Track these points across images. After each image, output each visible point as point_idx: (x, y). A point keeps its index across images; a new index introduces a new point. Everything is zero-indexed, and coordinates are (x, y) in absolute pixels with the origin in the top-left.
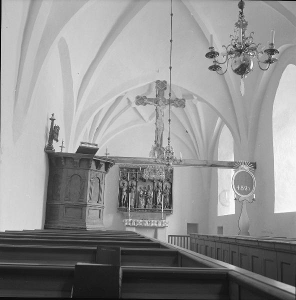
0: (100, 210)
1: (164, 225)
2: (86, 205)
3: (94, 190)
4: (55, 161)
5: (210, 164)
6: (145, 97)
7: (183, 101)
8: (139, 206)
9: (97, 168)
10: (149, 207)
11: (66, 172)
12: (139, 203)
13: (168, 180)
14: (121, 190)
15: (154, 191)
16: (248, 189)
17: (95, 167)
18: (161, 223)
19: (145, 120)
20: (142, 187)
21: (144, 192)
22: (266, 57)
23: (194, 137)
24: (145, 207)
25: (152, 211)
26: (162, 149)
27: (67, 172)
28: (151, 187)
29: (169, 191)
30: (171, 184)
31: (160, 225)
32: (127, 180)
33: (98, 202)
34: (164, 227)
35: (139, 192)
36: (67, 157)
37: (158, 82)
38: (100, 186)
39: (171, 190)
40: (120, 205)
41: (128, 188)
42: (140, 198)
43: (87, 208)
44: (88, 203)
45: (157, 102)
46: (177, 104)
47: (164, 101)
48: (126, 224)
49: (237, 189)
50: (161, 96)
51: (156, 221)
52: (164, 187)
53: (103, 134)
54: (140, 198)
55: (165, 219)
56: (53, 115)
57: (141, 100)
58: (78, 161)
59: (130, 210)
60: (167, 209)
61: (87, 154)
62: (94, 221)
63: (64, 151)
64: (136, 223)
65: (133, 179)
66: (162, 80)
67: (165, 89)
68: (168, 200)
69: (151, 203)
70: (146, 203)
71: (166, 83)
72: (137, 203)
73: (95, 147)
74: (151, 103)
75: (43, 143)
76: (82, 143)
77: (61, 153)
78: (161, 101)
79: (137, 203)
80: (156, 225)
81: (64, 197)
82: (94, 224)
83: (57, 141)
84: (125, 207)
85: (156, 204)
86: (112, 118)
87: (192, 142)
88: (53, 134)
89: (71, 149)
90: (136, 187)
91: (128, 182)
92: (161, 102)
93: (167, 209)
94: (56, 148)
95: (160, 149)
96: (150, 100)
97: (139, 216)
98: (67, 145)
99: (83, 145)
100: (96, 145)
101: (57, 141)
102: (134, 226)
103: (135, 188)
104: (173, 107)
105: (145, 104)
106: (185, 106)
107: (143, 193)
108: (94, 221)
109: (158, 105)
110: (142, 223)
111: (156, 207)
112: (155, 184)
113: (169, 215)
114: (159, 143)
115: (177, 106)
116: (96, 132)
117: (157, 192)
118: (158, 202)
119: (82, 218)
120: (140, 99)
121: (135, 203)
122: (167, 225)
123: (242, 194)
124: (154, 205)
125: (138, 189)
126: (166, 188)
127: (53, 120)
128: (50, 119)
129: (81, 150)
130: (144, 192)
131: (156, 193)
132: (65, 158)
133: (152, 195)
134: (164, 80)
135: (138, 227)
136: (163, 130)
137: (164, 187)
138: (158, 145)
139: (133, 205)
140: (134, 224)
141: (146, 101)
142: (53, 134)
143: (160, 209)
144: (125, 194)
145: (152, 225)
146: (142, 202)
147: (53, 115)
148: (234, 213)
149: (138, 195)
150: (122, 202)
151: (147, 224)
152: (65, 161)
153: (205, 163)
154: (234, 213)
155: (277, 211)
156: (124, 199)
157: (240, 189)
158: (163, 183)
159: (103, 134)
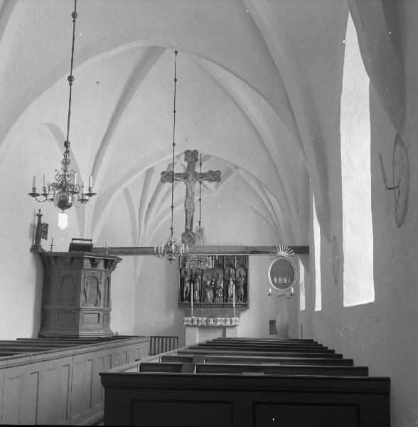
0: (99, 315)
1: (234, 324)
2: (79, 310)
3: (90, 292)
4: (46, 262)
8: (205, 300)
10: (220, 300)
12: (206, 295)
14: (182, 280)
15: (224, 280)
17: (90, 265)
18: (229, 321)
19: (208, 189)
21: (212, 281)
22: (42, 198)
23: (271, 205)
24: (213, 301)
26: (192, 235)
28: (221, 276)
29: (243, 280)
30: (247, 270)
32: (234, 268)
33: (95, 305)
35: (206, 282)
36: (58, 257)
37: (187, 152)
38: (98, 286)
39: (246, 278)
40: (182, 299)
41: (191, 277)
44: (82, 307)
46: (211, 177)
47: (195, 174)
48: (186, 323)
50: (192, 170)
51: (223, 319)
52: (238, 275)
55: (238, 316)
56: (40, 210)
57: (169, 176)
58: (69, 260)
60: (241, 303)
61: (80, 250)
62: (91, 326)
63: (54, 250)
64: (198, 321)
66: (191, 149)
67: (196, 160)
68: (242, 291)
69: (220, 295)
70: (215, 295)
71: (197, 153)
72: (203, 295)
74: (179, 179)
75: (29, 243)
76: (73, 239)
77: (51, 252)
80: (223, 324)
82: (90, 330)
83: (46, 239)
85: (227, 297)
87: (270, 213)
89: (62, 247)
90: (202, 276)
92: (191, 177)
93: (241, 303)
94: (45, 245)
95: (189, 236)
96: (179, 175)
97: (206, 313)
99: (74, 242)
100: (91, 240)
101: (46, 239)
102: (195, 326)
103: (200, 277)
104: (206, 182)
106: (220, 179)
107: (211, 284)
108: (91, 326)
110: (206, 321)
112: (226, 271)
114: (189, 227)
115: (210, 180)
116: (148, 210)
117: (229, 281)
118: (230, 295)
119: (75, 324)
121: (200, 294)
122: (237, 324)
123: (281, 288)
124: (225, 297)
125: (205, 279)
126: (240, 276)
127: (40, 216)
128: (37, 215)
129: (73, 247)
130: (212, 281)
131: (227, 283)
132: (55, 257)
133: (222, 285)
134: (195, 149)
137: (238, 275)
138: (187, 230)
139: (197, 298)
140: (196, 323)
144: (188, 285)
145: (219, 324)
146: (210, 295)
147: (40, 210)
148: (371, 299)
149: (204, 286)
151: (212, 322)
152: (56, 262)
153: (244, 250)
154: (371, 299)
155: (346, 304)
156: (187, 291)
158: (235, 269)
159: (157, 213)
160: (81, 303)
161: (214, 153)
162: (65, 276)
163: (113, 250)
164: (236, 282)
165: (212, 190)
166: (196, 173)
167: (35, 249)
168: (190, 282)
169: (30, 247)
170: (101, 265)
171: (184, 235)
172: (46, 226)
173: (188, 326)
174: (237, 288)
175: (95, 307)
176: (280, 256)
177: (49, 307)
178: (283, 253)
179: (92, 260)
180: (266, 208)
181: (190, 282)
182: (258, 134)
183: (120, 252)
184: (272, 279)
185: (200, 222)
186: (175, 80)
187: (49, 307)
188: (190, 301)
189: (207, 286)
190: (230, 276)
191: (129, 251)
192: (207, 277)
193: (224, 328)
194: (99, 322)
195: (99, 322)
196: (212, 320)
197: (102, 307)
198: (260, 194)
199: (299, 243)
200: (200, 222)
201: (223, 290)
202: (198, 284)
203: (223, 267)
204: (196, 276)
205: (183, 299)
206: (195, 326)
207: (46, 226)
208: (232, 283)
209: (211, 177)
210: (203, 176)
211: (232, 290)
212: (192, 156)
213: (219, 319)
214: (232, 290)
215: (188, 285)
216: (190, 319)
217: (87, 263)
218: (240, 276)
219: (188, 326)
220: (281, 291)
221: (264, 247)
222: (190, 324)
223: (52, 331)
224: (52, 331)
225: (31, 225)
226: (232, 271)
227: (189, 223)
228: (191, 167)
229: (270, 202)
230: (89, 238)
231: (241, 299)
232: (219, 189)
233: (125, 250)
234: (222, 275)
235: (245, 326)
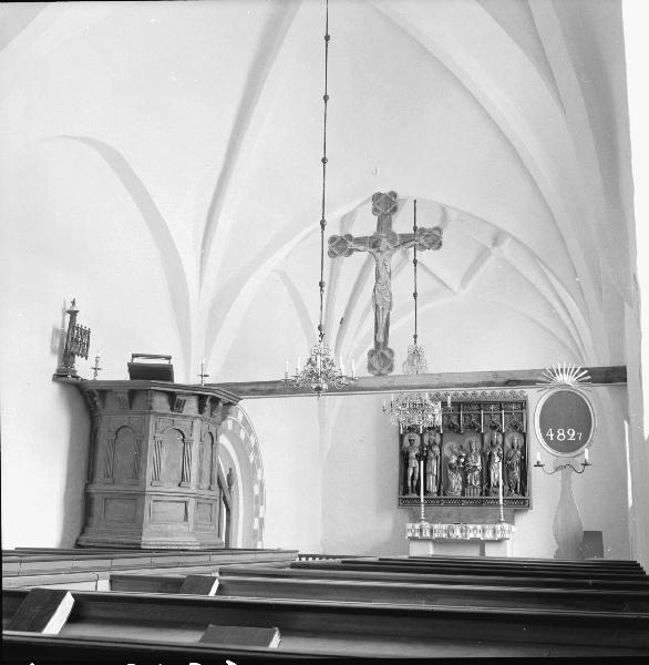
2: (142, 494)
4: (88, 400)
5: (503, 380)
6: (349, 237)
7: (437, 233)
9: (172, 409)
11: (111, 418)
12: (448, 484)
13: (516, 427)
14: (405, 458)
15: (483, 455)
16: (576, 436)
18: (491, 532)
19: (450, 289)
20: (455, 445)
24: (463, 493)
25: (480, 503)
26: (386, 353)
27: (120, 418)
28: (476, 445)
29: (519, 452)
30: (525, 435)
31: (489, 536)
32: (500, 431)
34: (500, 541)
39: (524, 449)
40: (406, 491)
41: (421, 450)
42: (449, 472)
43: (148, 501)
44: (148, 488)
45: (375, 245)
46: (422, 241)
47: (392, 237)
48: (410, 535)
49: (547, 439)
51: (479, 527)
52: (508, 444)
53: (357, 333)
54: (449, 472)
55: (511, 521)
56: (73, 303)
58: (126, 397)
59: (501, 502)
60: (516, 496)
61: (150, 376)
64: (431, 531)
65: (494, 428)
66: (385, 190)
70: (465, 483)
72: (443, 483)
73: (166, 362)
74: (361, 248)
75: (53, 364)
76: (134, 356)
77: (94, 382)
78: (384, 240)
79: (443, 483)
80: (479, 536)
81: (102, 476)
84: (415, 496)
85: (489, 486)
86: (561, 287)
88: (73, 342)
91: (422, 436)
92: (384, 243)
94: (83, 369)
95: (383, 355)
96: (360, 241)
97: (448, 516)
98: (107, 364)
99: (136, 360)
100: (169, 358)
102: (427, 540)
103: (436, 449)
105: (350, 252)
106: (441, 244)
107: (458, 462)
108: (175, 528)
109: (379, 251)
110: (447, 531)
111: (487, 494)
112: (486, 438)
113: (526, 510)
114: (381, 339)
117: (491, 455)
119: (137, 522)
120: (337, 244)
121: (439, 484)
125: (446, 452)
126: (513, 447)
127: (73, 314)
128: (69, 312)
129: (136, 371)
130: (460, 457)
133: (478, 464)
135: (438, 542)
136: (390, 309)
137: (508, 444)
138: (377, 344)
139: (433, 488)
140: (428, 535)
141: (351, 244)
142: (73, 342)
143: (415, 496)
145: (471, 535)
146: (456, 480)
149: (445, 467)
150: (410, 482)
151: (457, 534)
153: (491, 379)
157: (555, 437)
158: (503, 435)
159: (357, 333)
160: (148, 483)
161: (427, 191)
162: (119, 430)
163: (241, 388)
164: (505, 459)
165: (456, 290)
166: (393, 234)
167: (63, 376)
168: (419, 457)
169: (54, 372)
170: (191, 406)
171: (372, 354)
172: (87, 333)
173: (413, 539)
174: (507, 469)
175: (178, 489)
176: (560, 386)
177: (93, 489)
178: (568, 379)
179: (172, 397)
180: (573, 341)
181: (419, 457)
182: (507, 142)
183: (253, 390)
184: (544, 432)
185: (415, 337)
186: (327, 38)
187: (93, 489)
188: (419, 494)
189: (450, 465)
190: (492, 445)
191: (270, 387)
192: (451, 449)
193: (481, 544)
194: (186, 519)
195: (186, 519)
196: (457, 529)
197: (193, 489)
198: (544, 289)
199: (604, 361)
200: (415, 337)
201: (481, 473)
202: (434, 463)
203: (479, 431)
204: (430, 447)
205: (408, 492)
206: (427, 540)
207: (87, 333)
208: (497, 459)
209: (422, 241)
210: (406, 240)
211: (497, 473)
212: (386, 205)
213: (471, 527)
214: (497, 473)
215: (414, 463)
216: (417, 526)
217: (161, 403)
218: (513, 447)
219: (413, 539)
220: (564, 458)
221: (532, 372)
222: (417, 535)
223: (92, 536)
224: (92, 536)
225: (56, 331)
226: (498, 437)
227: (381, 330)
228: (384, 221)
229: (564, 306)
230: (167, 354)
231: (516, 490)
232: (468, 289)
233: (263, 387)
234: (479, 444)
235: (526, 539)
